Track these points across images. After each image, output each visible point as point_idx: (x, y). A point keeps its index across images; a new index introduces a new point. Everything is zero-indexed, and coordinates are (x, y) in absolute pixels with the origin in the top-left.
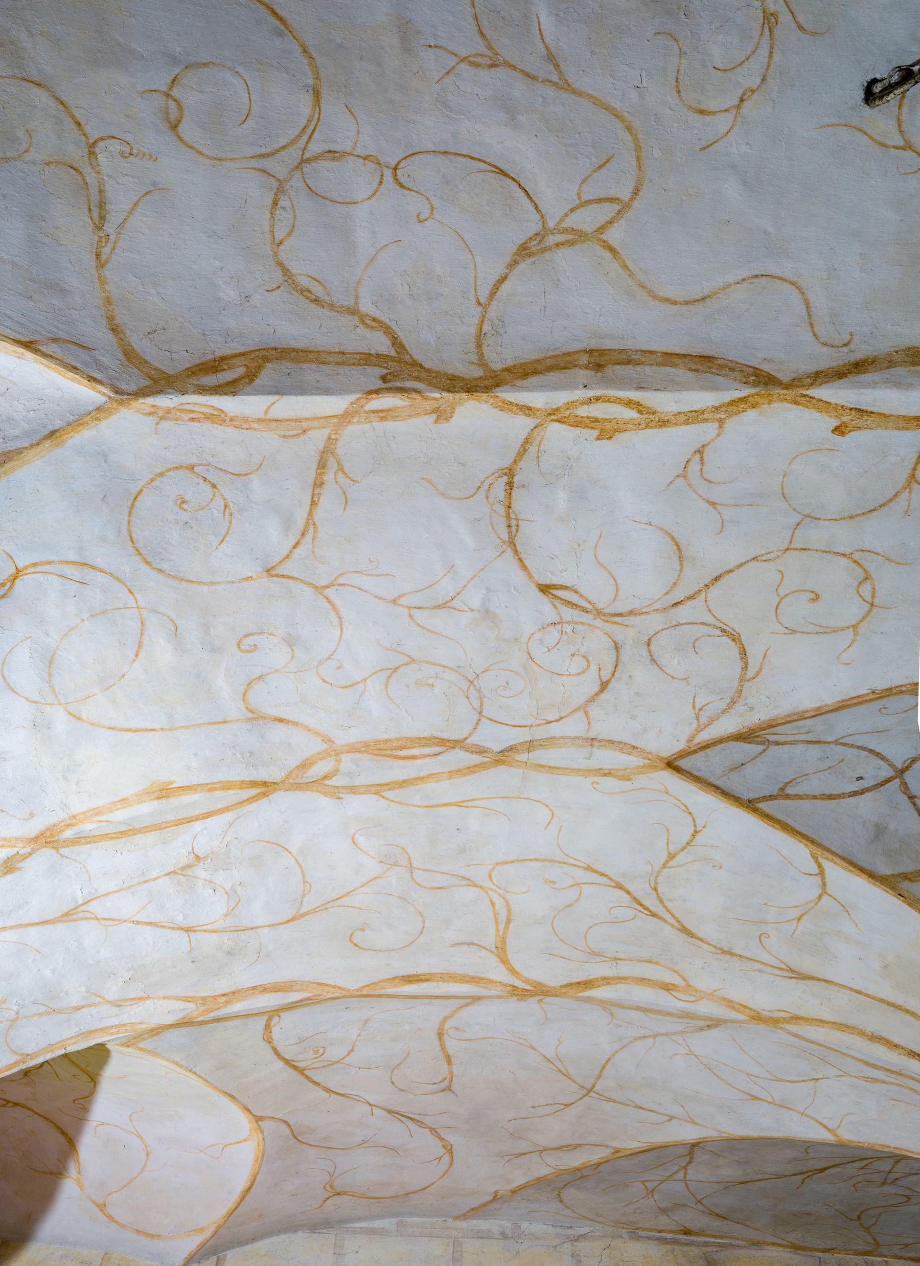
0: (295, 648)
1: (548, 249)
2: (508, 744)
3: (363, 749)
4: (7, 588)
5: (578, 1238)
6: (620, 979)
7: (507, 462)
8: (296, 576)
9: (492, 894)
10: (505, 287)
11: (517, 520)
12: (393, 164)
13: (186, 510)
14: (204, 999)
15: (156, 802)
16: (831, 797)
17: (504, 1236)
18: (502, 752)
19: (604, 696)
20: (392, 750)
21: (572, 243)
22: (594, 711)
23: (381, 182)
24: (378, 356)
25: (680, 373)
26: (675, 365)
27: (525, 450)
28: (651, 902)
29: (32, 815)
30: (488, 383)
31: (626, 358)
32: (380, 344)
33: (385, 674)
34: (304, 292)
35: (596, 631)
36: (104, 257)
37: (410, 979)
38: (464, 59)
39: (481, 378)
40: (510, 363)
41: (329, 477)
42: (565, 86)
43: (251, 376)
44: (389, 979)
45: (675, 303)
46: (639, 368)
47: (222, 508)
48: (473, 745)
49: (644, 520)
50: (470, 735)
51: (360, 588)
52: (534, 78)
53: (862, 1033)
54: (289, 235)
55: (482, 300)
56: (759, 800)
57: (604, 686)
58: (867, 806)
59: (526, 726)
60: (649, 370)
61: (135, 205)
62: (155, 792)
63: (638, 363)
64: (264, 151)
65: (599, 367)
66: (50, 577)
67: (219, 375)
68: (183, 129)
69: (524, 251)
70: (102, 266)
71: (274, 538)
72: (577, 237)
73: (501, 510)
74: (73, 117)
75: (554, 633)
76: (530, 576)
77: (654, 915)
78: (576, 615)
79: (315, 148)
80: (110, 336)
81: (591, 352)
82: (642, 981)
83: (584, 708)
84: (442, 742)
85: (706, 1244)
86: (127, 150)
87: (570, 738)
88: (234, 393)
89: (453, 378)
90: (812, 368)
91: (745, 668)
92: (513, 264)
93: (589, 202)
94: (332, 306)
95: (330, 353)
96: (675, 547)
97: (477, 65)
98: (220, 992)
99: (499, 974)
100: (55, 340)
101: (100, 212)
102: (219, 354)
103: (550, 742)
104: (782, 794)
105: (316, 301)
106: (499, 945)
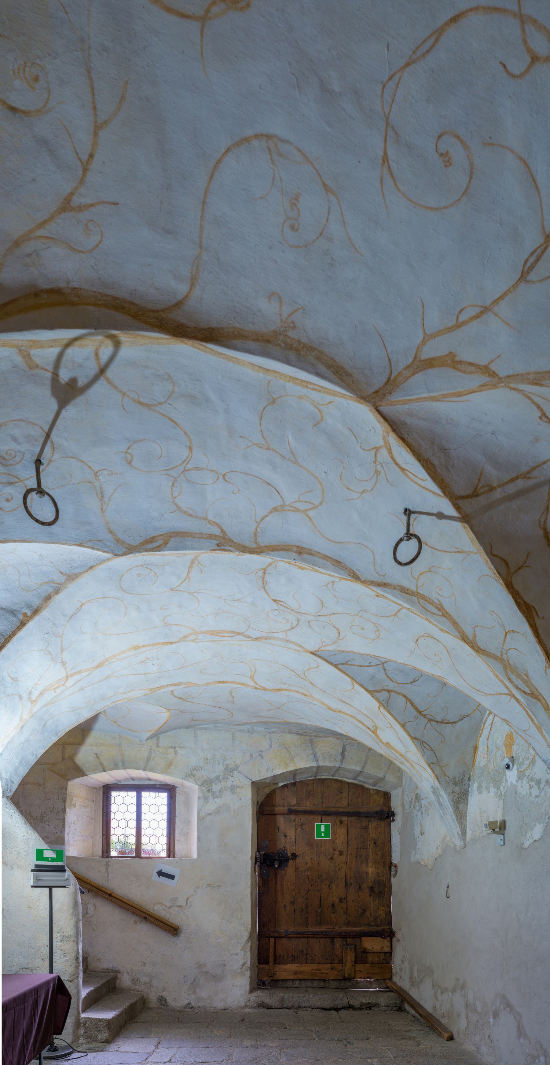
1: (285, 510)
2: (258, 636)
5: (272, 733)
6: (290, 690)
10: (267, 519)
12: (223, 473)
16: (361, 666)
17: (249, 731)
19: (293, 630)
21: (294, 511)
22: (289, 633)
23: (218, 479)
24: (216, 536)
25: (328, 564)
26: (327, 561)
28: (303, 676)
29: (94, 660)
30: (258, 550)
31: (310, 552)
32: (216, 531)
34: (185, 512)
36: (104, 509)
38: (255, 444)
39: (255, 548)
40: (267, 544)
42: (296, 462)
43: (166, 543)
45: (330, 540)
46: (315, 558)
52: (284, 457)
53: (357, 720)
54: (179, 495)
55: (257, 521)
56: (338, 664)
58: (371, 670)
60: (318, 559)
61: (115, 490)
63: (314, 556)
64: (168, 468)
65: (300, 553)
67: (153, 544)
68: (133, 463)
69: (275, 509)
70: (104, 512)
72: (297, 510)
74: (87, 465)
75: (277, 612)
76: (270, 597)
78: (285, 609)
79: (189, 466)
80: (110, 535)
81: (298, 547)
82: (298, 692)
83: (286, 631)
84: (234, 633)
85: (311, 736)
86: (111, 473)
88: (159, 551)
89: (244, 547)
90: (371, 579)
91: (339, 636)
92: (271, 513)
93: (302, 501)
94: (196, 517)
95: (196, 533)
97: (260, 447)
99: (252, 684)
100: (89, 541)
101: (101, 495)
102: (152, 536)
103: (273, 638)
104: (346, 663)
105: (190, 515)
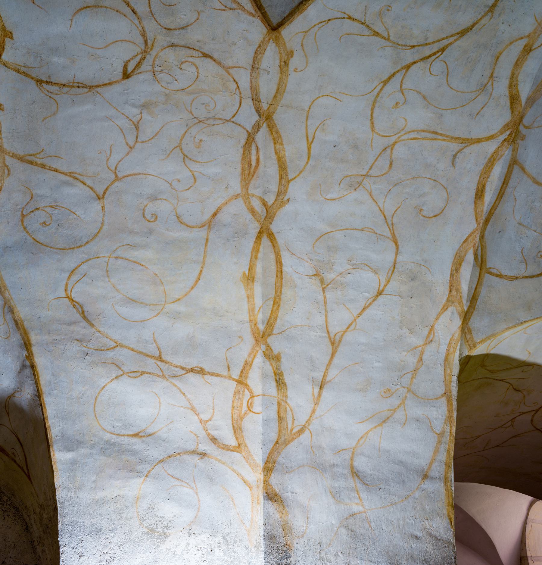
0: (158, 198)
3: (247, 182)
4: (77, 305)
7: (33, 83)
8: (105, 187)
9: (403, 138)
11: (73, 83)
13: (50, 223)
14: (448, 301)
15: (255, 284)
18: (259, 115)
20: (250, 168)
27: (24, 73)
33: (187, 160)
35: (160, 54)
37: (480, 194)
41: (39, 161)
44: (475, 206)
47: (52, 209)
48: (253, 128)
49: (69, 22)
50: (245, 129)
51: (120, 161)
57: (206, 55)
59: (241, 100)
62: (248, 282)
66: (75, 287)
71: (74, 192)
73: (65, 89)
76: (117, 82)
77: (443, 50)
87: (251, 80)
96: (88, 9)
98: (447, 293)
106: (461, 141)
